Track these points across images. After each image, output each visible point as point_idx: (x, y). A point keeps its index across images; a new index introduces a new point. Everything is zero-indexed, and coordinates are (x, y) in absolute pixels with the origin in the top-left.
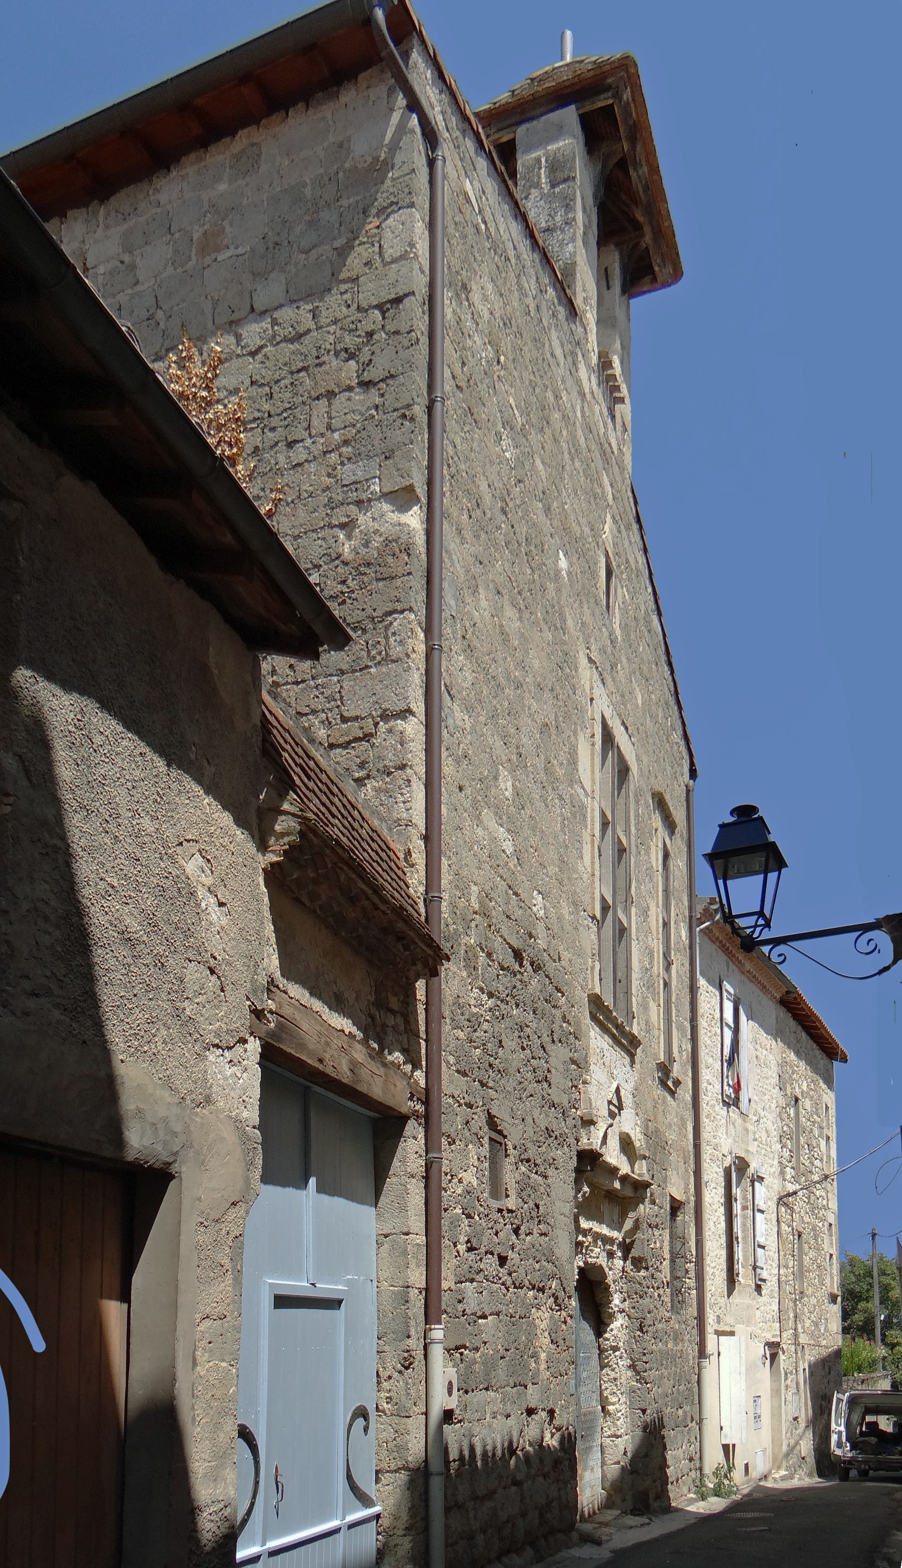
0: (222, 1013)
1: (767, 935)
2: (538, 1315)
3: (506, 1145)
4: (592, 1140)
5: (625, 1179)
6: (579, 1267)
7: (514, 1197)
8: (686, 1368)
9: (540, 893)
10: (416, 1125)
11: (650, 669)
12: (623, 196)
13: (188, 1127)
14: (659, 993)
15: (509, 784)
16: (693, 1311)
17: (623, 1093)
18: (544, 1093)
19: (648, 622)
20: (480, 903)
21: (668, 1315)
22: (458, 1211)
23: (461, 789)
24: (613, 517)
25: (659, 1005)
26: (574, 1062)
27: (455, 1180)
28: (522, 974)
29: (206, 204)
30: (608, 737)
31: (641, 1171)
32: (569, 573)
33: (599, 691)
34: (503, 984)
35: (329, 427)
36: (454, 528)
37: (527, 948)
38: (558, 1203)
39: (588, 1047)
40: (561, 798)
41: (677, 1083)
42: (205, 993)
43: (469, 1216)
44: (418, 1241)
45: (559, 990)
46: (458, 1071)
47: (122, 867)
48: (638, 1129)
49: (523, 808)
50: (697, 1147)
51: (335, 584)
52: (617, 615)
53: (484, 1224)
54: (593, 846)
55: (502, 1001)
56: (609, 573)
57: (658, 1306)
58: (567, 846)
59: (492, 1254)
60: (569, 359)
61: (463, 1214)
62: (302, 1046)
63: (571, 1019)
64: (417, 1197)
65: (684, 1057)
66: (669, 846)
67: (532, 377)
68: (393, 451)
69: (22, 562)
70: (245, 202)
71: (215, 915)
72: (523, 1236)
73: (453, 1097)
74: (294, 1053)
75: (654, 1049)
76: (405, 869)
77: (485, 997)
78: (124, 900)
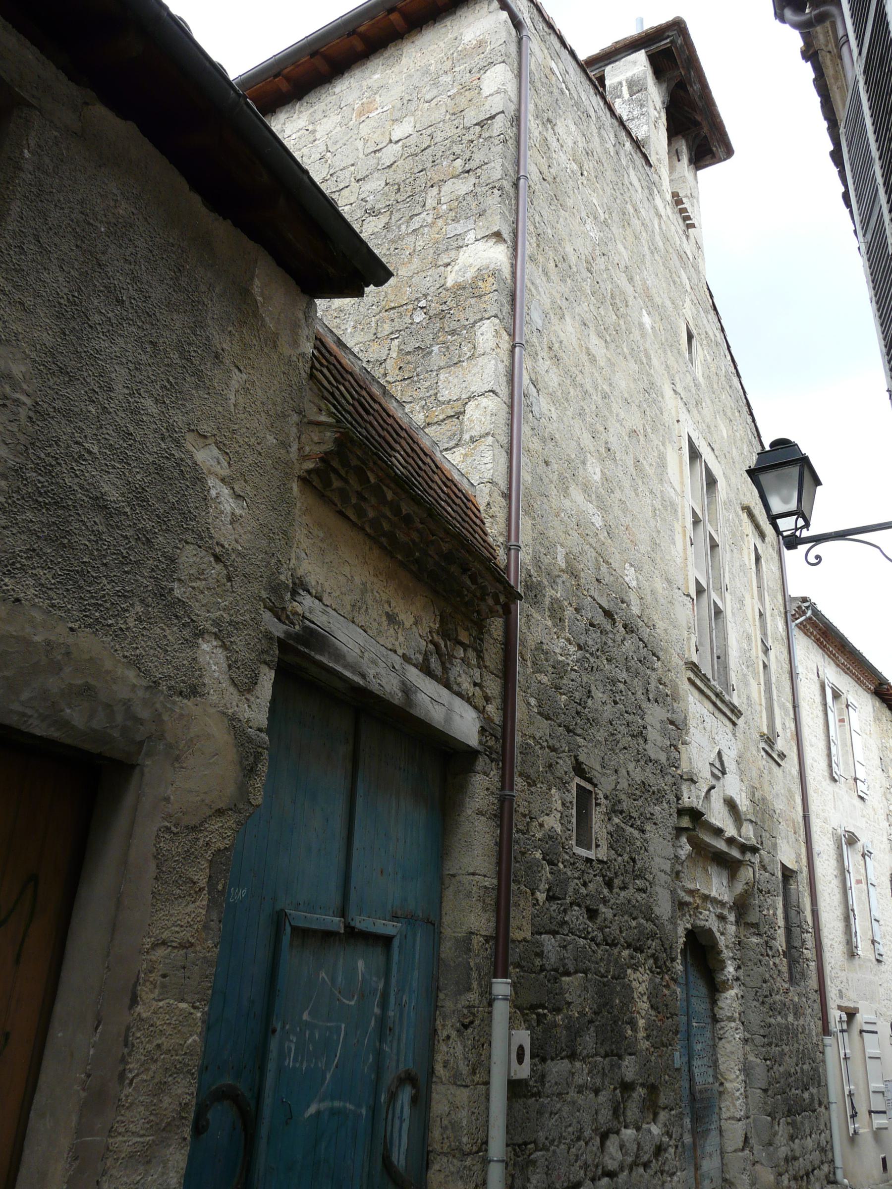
0: (226, 603)
1: (805, 534)
2: (635, 976)
3: (596, 794)
4: (691, 797)
5: (731, 841)
6: (686, 929)
7: (605, 848)
8: (810, 1046)
9: (631, 565)
10: (488, 761)
11: (733, 414)
12: (686, 108)
13: (160, 715)
14: (758, 673)
15: (598, 470)
16: (813, 983)
17: (725, 758)
18: (640, 748)
19: (729, 381)
20: (567, 562)
21: (786, 986)
22: (538, 855)
23: (547, 463)
24: (692, 300)
25: (759, 684)
26: (672, 723)
27: (535, 823)
28: (614, 634)
29: (365, 87)
30: (695, 454)
31: (748, 833)
32: (653, 328)
33: (684, 416)
34: (593, 639)
35: (439, 203)
36: (540, 269)
37: (618, 611)
38: (657, 859)
39: (687, 710)
40: (651, 492)
41: (782, 756)
42: (205, 579)
43: (551, 863)
44: (486, 884)
45: (654, 654)
46: (540, 713)
47: (107, 437)
48: (744, 795)
49: (612, 492)
50: (806, 818)
51: (438, 305)
52: (700, 367)
53: (569, 873)
54: (685, 535)
55: (592, 654)
56: (690, 337)
57: (775, 976)
58: (659, 532)
59: (579, 905)
60: (646, 190)
61: (544, 859)
62: (338, 656)
63: (667, 682)
64: (487, 836)
65: (789, 734)
66: (760, 551)
67: (613, 191)
68: (485, 211)
69: (27, 154)
70: (390, 81)
71: (229, 504)
72: (616, 890)
73: (534, 738)
74: (326, 662)
75: (756, 719)
76: (485, 520)
77: (572, 649)
78: (105, 468)
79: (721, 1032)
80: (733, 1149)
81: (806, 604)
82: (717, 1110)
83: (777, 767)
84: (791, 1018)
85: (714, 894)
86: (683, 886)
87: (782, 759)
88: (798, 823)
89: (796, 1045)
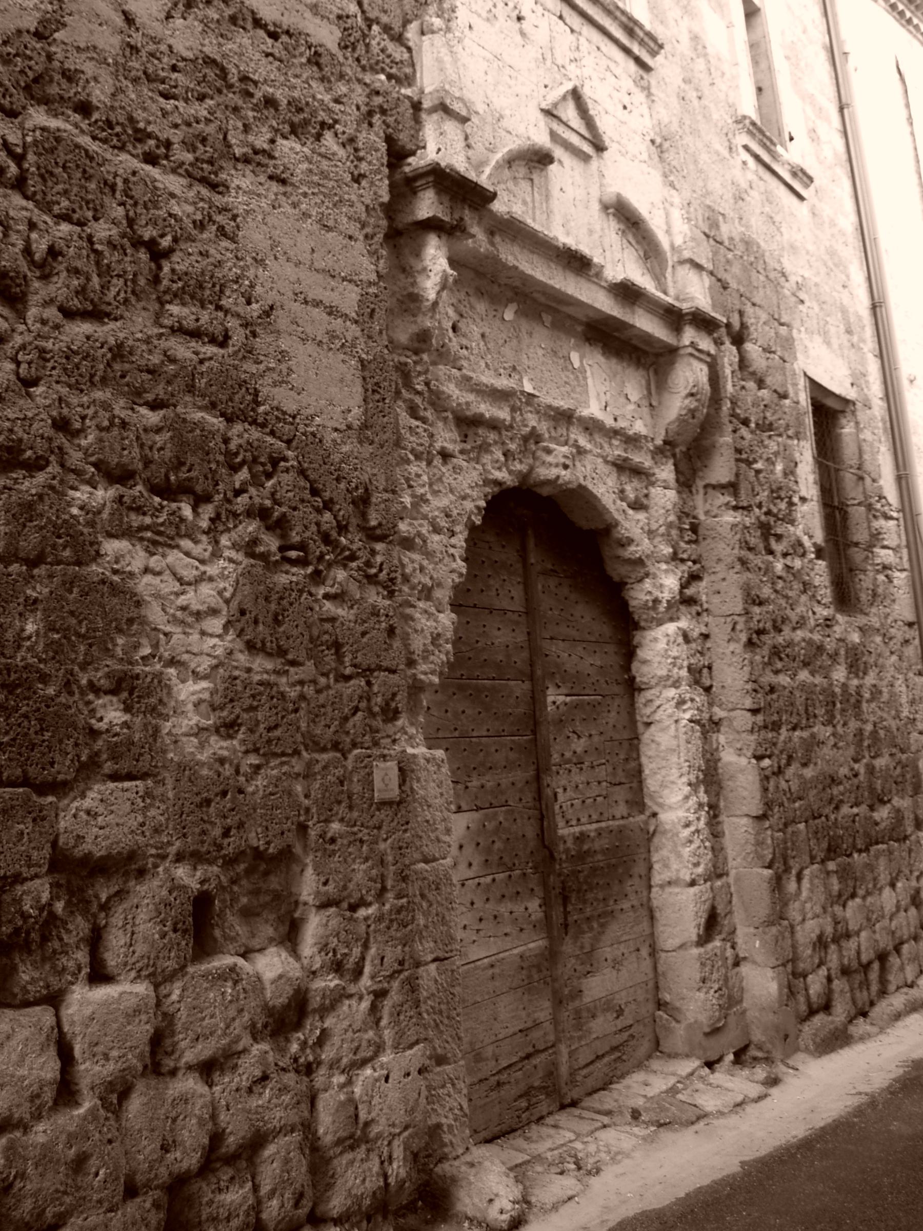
5: (627, 293)
8: (893, 724)
50: (876, 307)
79: (648, 711)
80: (677, 942)
82: (639, 869)
84: (840, 674)
85: (593, 409)
86: (469, 379)
88: (860, 318)
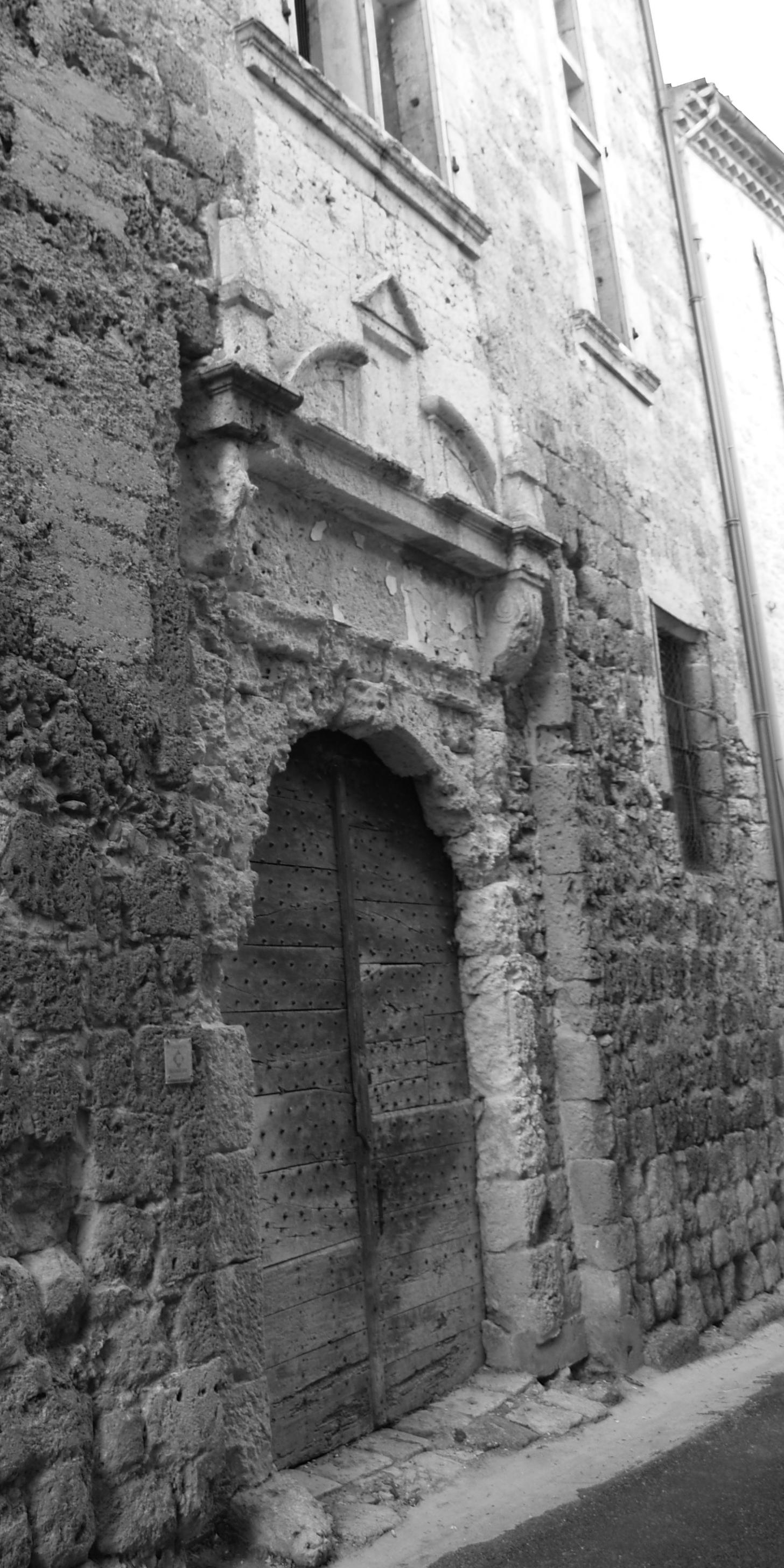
81: (706, 92)
83: (639, 405)
84: (690, 940)
85: (412, 641)
87: (653, 389)
88: (713, 538)
89: (705, 997)
